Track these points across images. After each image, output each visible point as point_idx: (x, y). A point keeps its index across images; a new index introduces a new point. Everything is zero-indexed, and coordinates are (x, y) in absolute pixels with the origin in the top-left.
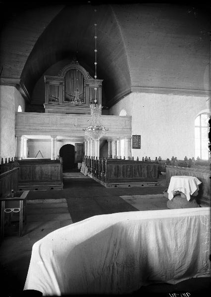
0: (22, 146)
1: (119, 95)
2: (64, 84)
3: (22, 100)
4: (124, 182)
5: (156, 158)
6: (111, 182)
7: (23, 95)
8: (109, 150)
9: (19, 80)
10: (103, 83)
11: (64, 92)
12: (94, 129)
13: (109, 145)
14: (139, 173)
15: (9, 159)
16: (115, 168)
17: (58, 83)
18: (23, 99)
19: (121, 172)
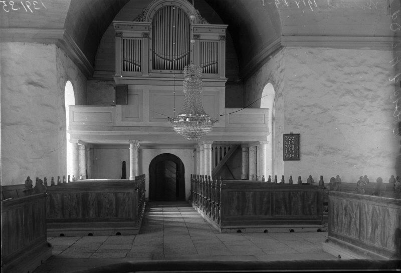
0: (201, 166)
1: (263, 54)
2: (151, 36)
3: (74, 72)
4: (257, 223)
5: (300, 178)
6: (230, 224)
7: (75, 61)
8: (243, 164)
9: (63, 32)
10: (228, 30)
11: (151, 52)
12: (187, 120)
13: (244, 154)
14: (286, 208)
15: (53, 179)
16: (238, 198)
17: (140, 35)
18: (76, 68)
19: (251, 205)
